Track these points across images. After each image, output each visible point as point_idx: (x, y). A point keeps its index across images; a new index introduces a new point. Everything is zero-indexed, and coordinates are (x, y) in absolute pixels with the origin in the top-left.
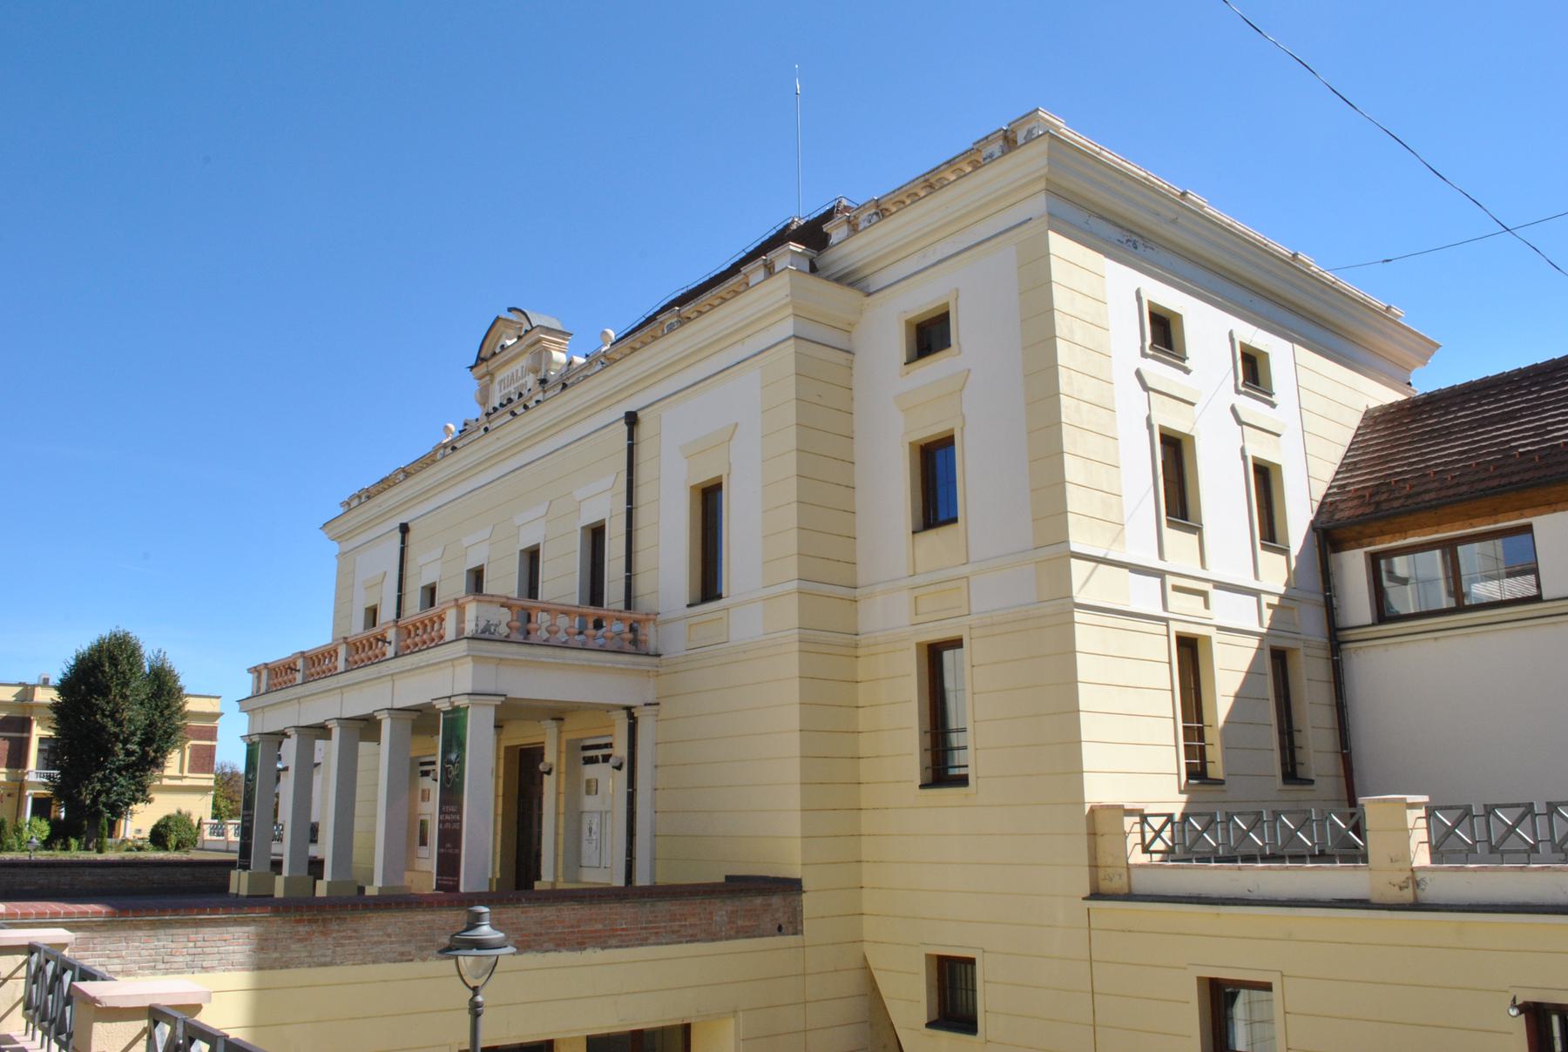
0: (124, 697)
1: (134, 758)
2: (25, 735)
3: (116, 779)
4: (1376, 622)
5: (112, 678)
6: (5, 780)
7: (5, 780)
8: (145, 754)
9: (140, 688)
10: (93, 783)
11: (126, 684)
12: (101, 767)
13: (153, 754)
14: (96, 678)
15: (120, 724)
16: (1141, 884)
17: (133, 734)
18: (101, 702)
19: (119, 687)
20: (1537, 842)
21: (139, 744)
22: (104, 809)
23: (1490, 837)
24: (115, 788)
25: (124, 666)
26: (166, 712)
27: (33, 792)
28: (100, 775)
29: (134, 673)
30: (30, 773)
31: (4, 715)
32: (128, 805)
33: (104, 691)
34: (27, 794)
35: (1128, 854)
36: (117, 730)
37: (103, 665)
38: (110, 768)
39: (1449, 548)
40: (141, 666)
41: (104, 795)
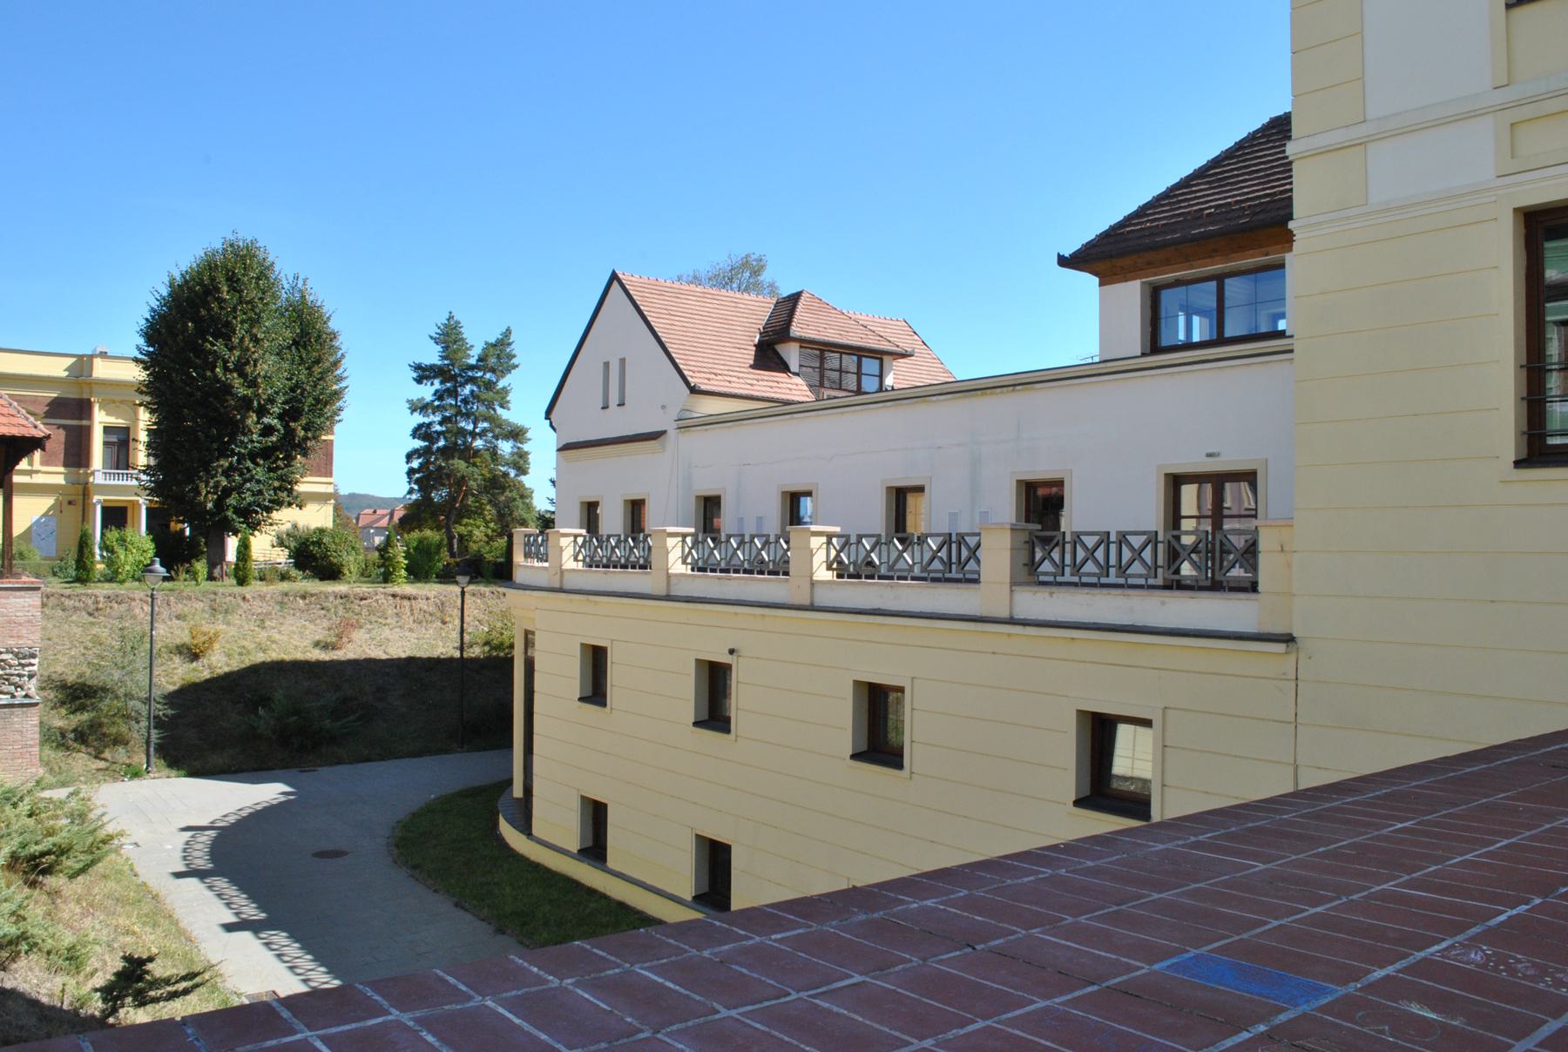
0: (256, 341)
1: (274, 439)
2: (84, 423)
3: (249, 470)
4: (1148, 351)
5: (234, 310)
6: (63, 482)
7: (63, 482)
8: (290, 433)
9: (275, 331)
10: (215, 476)
11: (255, 322)
12: (224, 452)
13: (303, 433)
14: (210, 310)
15: (253, 384)
16: (823, 598)
17: (271, 401)
18: (219, 346)
19: (246, 326)
20: (914, 564)
21: (280, 417)
22: (234, 516)
23: (922, 559)
24: (248, 485)
25: (251, 293)
26: (317, 370)
27: (102, 498)
28: (225, 463)
29: (267, 304)
30: (96, 473)
31: (55, 395)
32: (269, 510)
33: (224, 331)
34: (94, 501)
35: (814, 569)
36: (249, 392)
37: (218, 290)
38: (239, 454)
39: (1220, 278)
40: (275, 297)
41: (234, 495)
